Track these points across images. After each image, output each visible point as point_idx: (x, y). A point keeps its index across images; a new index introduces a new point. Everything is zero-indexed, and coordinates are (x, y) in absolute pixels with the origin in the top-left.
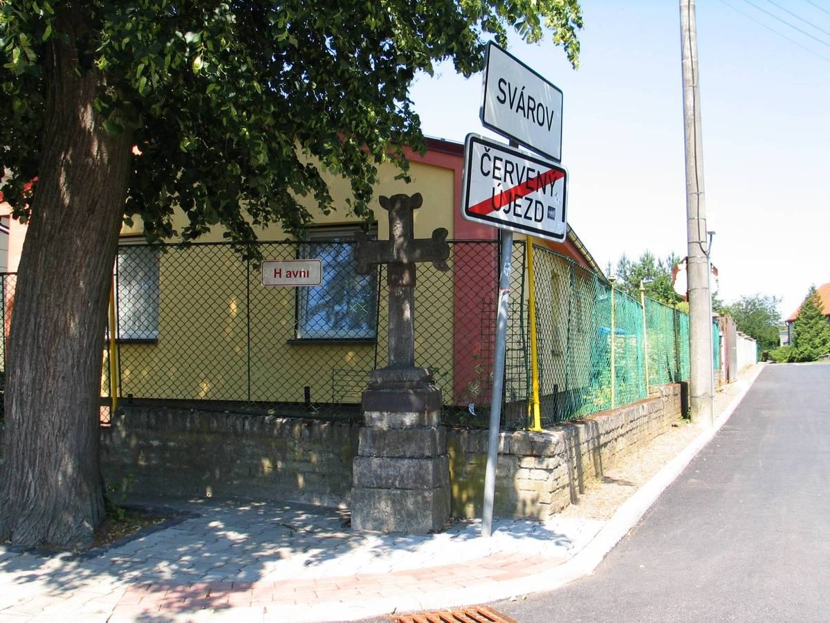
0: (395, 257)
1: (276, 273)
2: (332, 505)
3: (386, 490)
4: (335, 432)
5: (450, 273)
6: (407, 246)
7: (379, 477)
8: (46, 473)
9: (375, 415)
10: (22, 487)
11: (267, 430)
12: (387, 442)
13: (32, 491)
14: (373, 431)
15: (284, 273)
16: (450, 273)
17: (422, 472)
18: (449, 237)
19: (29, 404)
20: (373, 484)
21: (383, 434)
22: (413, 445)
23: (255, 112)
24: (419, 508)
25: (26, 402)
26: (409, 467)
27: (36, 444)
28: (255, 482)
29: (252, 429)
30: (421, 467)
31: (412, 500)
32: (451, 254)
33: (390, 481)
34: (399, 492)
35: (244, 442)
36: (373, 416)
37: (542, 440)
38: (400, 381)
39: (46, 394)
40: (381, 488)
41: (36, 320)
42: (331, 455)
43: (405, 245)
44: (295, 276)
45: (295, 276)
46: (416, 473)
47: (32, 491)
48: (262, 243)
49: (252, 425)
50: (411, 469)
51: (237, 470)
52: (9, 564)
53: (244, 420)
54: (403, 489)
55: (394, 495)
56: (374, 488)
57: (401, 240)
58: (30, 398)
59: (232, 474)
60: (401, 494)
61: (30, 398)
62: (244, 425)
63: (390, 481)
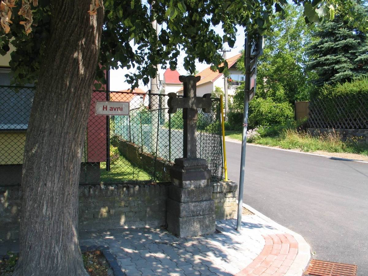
1: (106, 108)
2: (141, 226)
3: (196, 217)
4: (142, 190)
7: (193, 212)
8: (66, 245)
9: (188, 182)
10: (51, 257)
11: (104, 193)
12: (195, 195)
13: (59, 258)
14: (188, 190)
15: (108, 108)
17: (212, 206)
19: (57, 204)
20: (190, 215)
21: (192, 191)
22: (206, 195)
24: (210, 223)
25: (55, 203)
26: (206, 205)
27: (60, 228)
28: (97, 221)
29: (94, 193)
30: (211, 204)
31: (208, 219)
33: (198, 213)
34: (202, 217)
35: (90, 200)
36: (187, 183)
37: (234, 185)
38: (198, 165)
39: (67, 196)
40: (194, 216)
41: (63, 149)
42: (140, 202)
43: (195, 102)
44: (115, 110)
45: (115, 110)
46: (209, 207)
47: (59, 258)
48: (112, 92)
49: (95, 191)
50: (207, 206)
51: (86, 216)
53: (89, 189)
54: (203, 215)
55: (200, 218)
56: (191, 217)
58: (58, 200)
59: (83, 219)
60: (203, 218)
61: (58, 200)
62: (89, 191)
63: (198, 213)
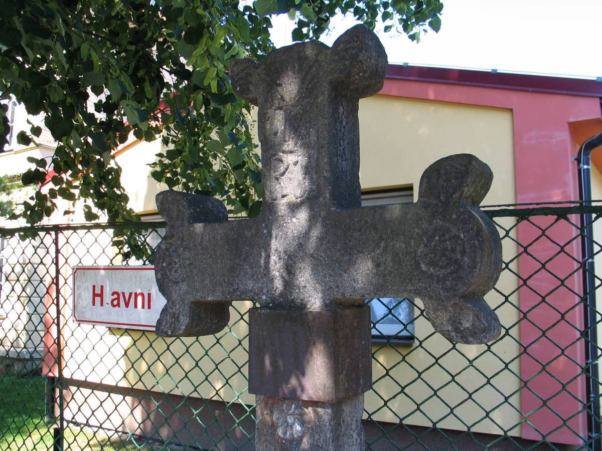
0: (278, 284)
5: (507, 348)
6: (321, 239)
15: (108, 298)
16: (507, 348)
18: (500, 193)
23: (223, 46)
32: (509, 250)
43: (315, 233)
44: (127, 305)
45: (127, 305)
52: (203, 426)
57: (303, 216)
